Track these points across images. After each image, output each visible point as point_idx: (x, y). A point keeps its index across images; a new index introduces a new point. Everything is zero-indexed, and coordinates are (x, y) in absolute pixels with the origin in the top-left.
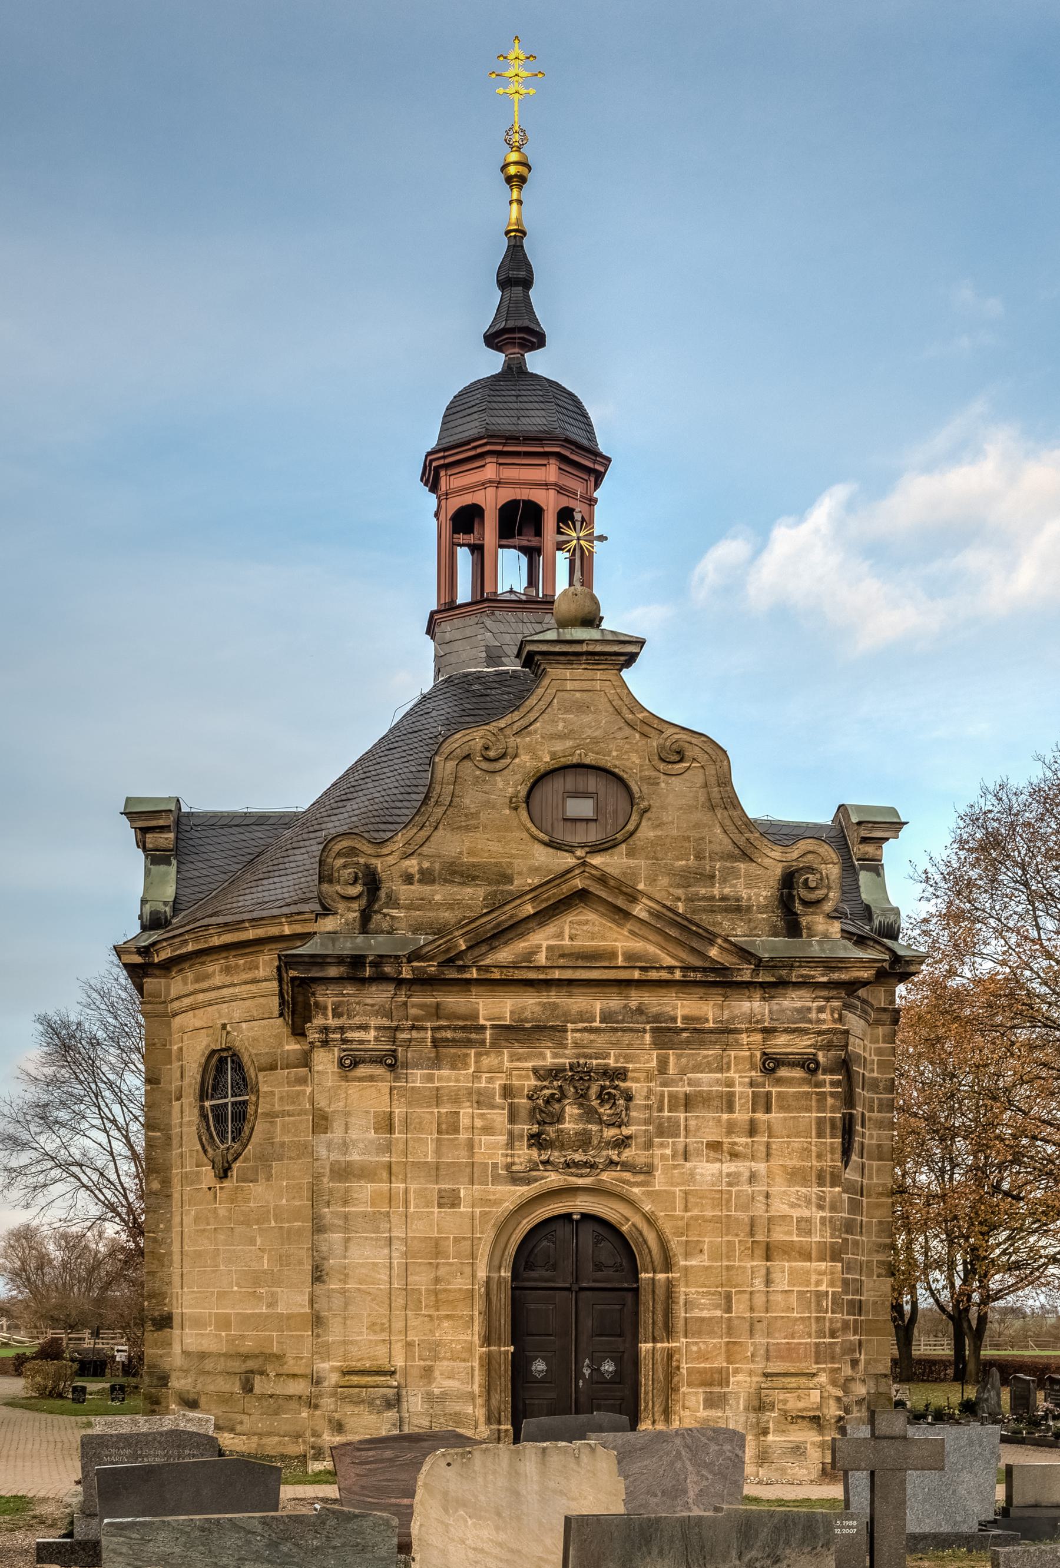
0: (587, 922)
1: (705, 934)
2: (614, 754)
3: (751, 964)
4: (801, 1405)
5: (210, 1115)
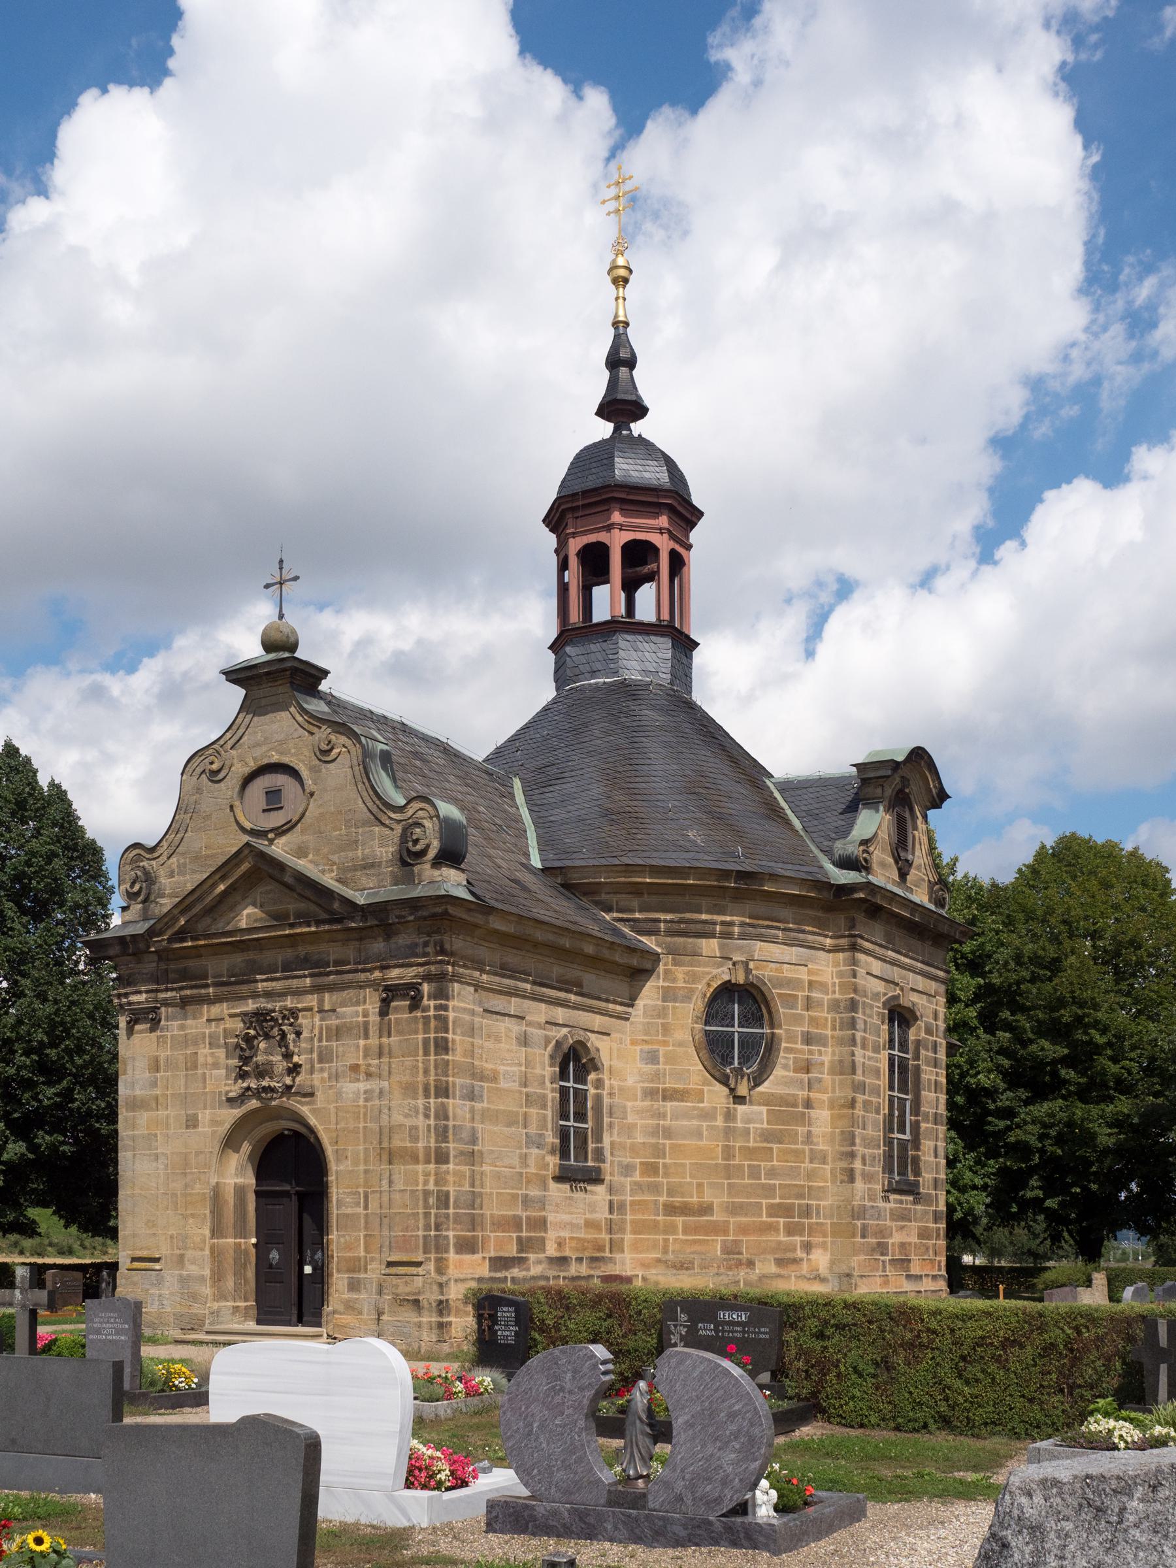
4: (408, 1289)
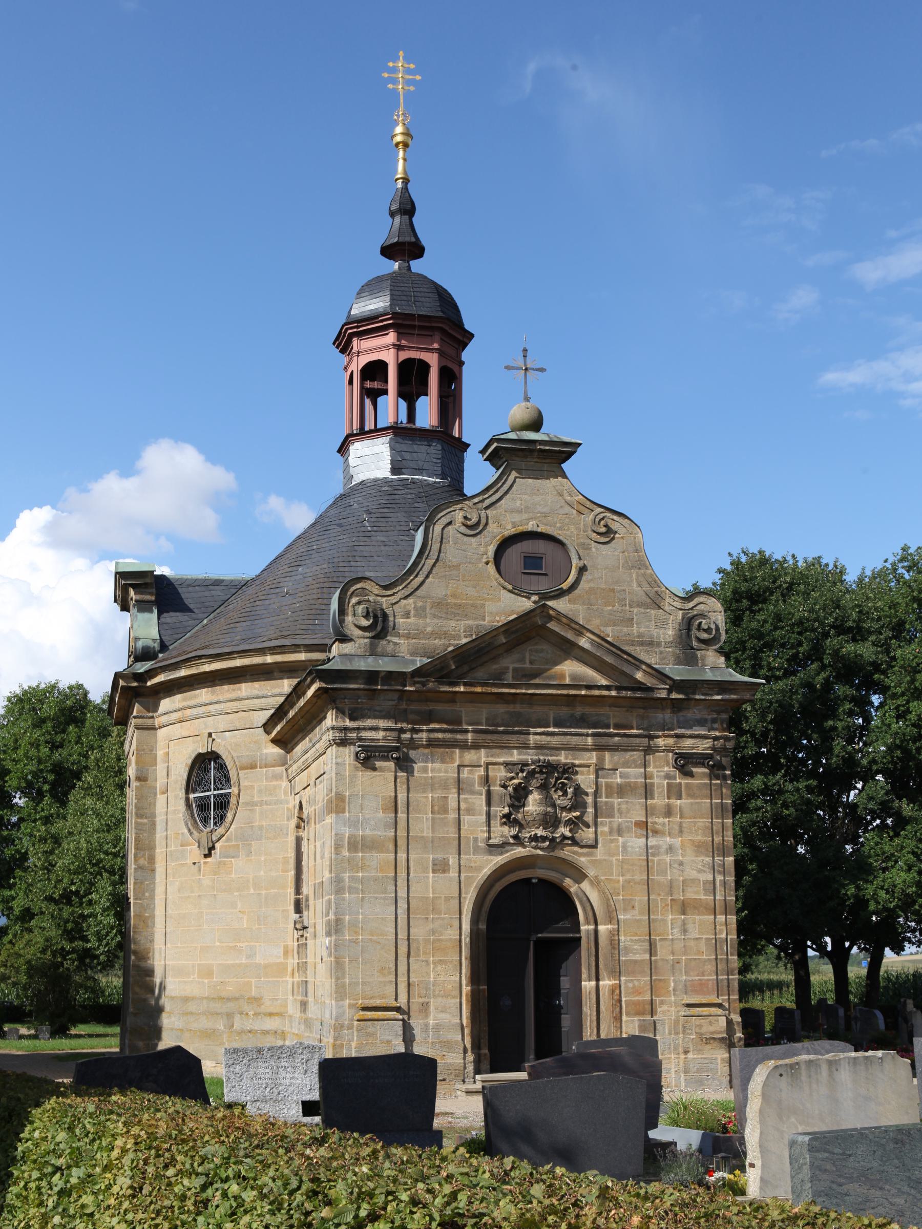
0: (542, 651)
1: (633, 661)
2: (558, 525)
3: (667, 684)
4: (712, 1029)
5: (194, 806)
